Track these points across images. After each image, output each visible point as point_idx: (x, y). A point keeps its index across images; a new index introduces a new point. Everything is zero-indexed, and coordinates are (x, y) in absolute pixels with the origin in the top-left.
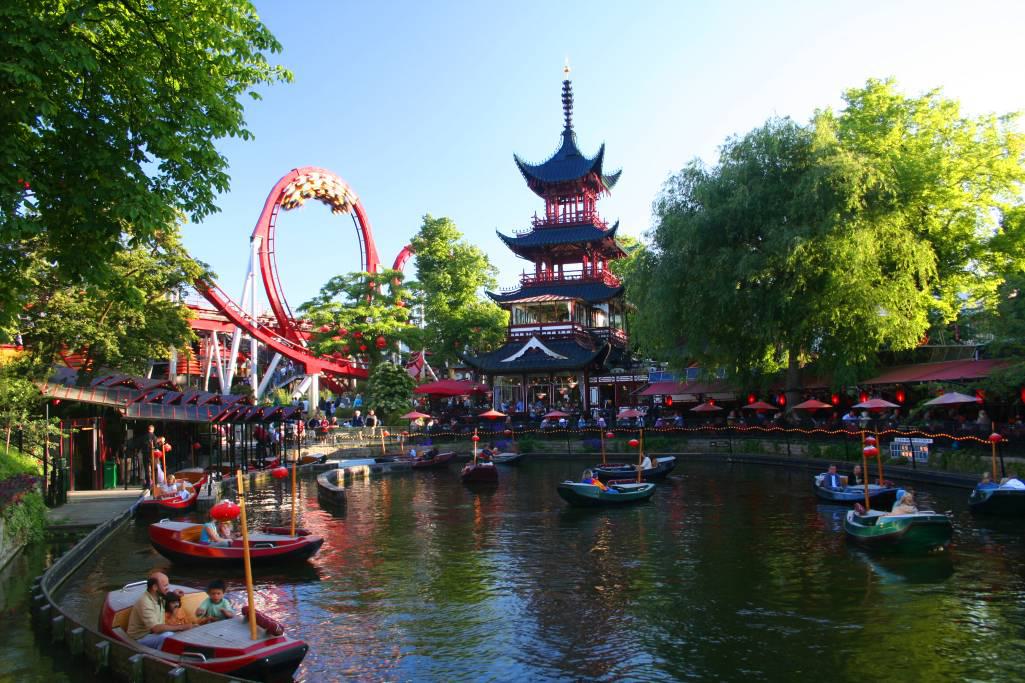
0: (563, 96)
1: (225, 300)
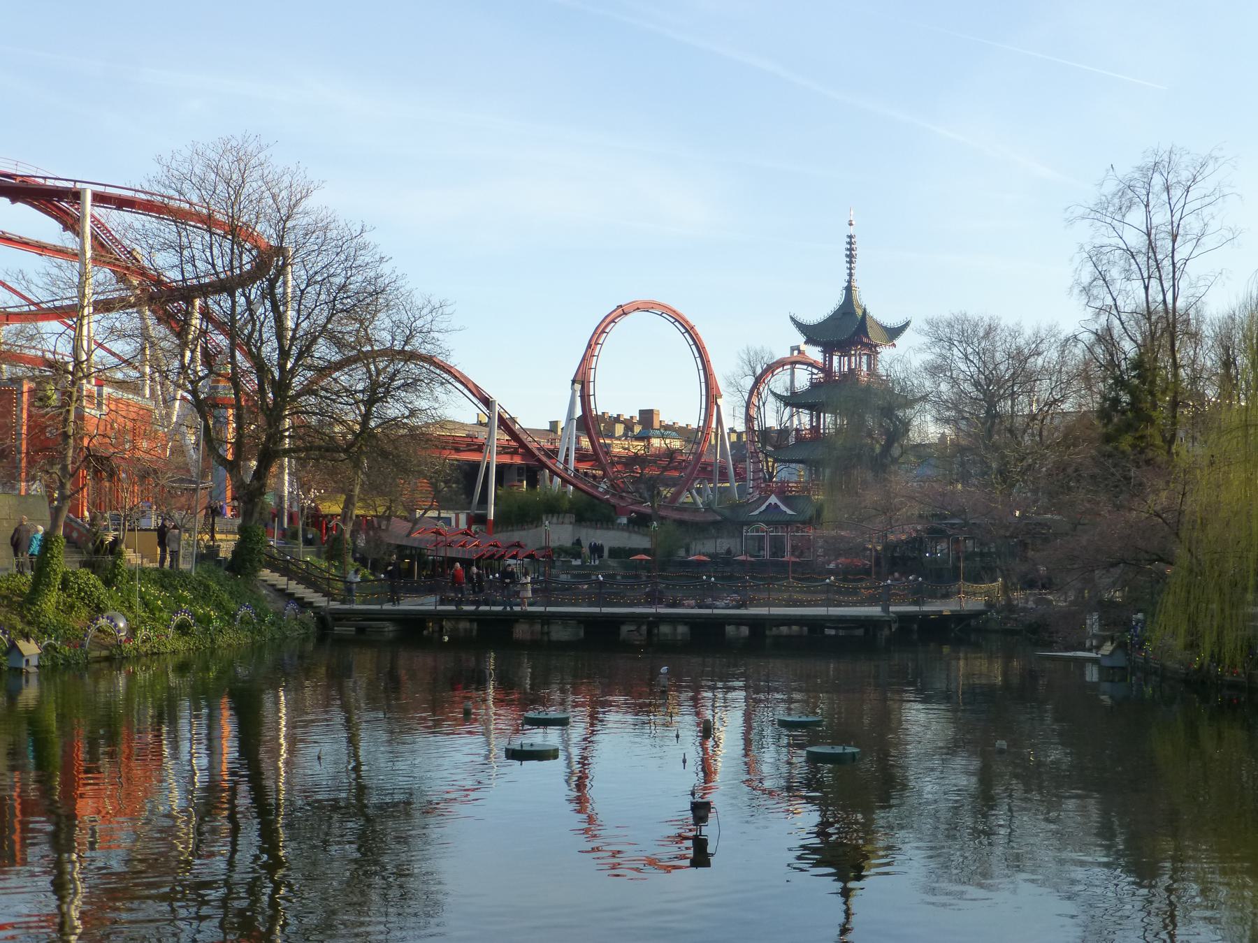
0: (848, 249)
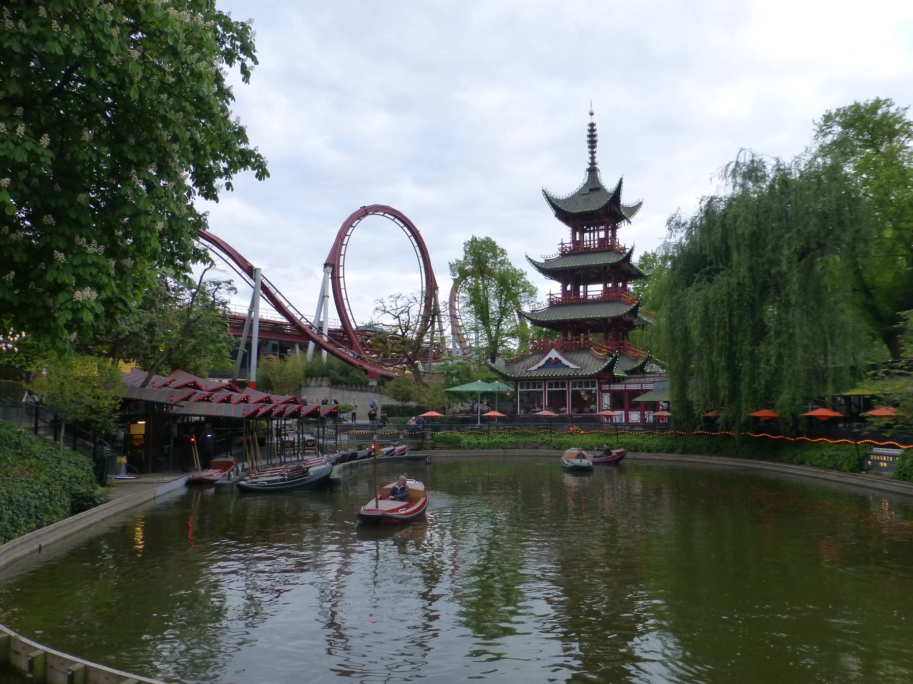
1: (299, 317)
